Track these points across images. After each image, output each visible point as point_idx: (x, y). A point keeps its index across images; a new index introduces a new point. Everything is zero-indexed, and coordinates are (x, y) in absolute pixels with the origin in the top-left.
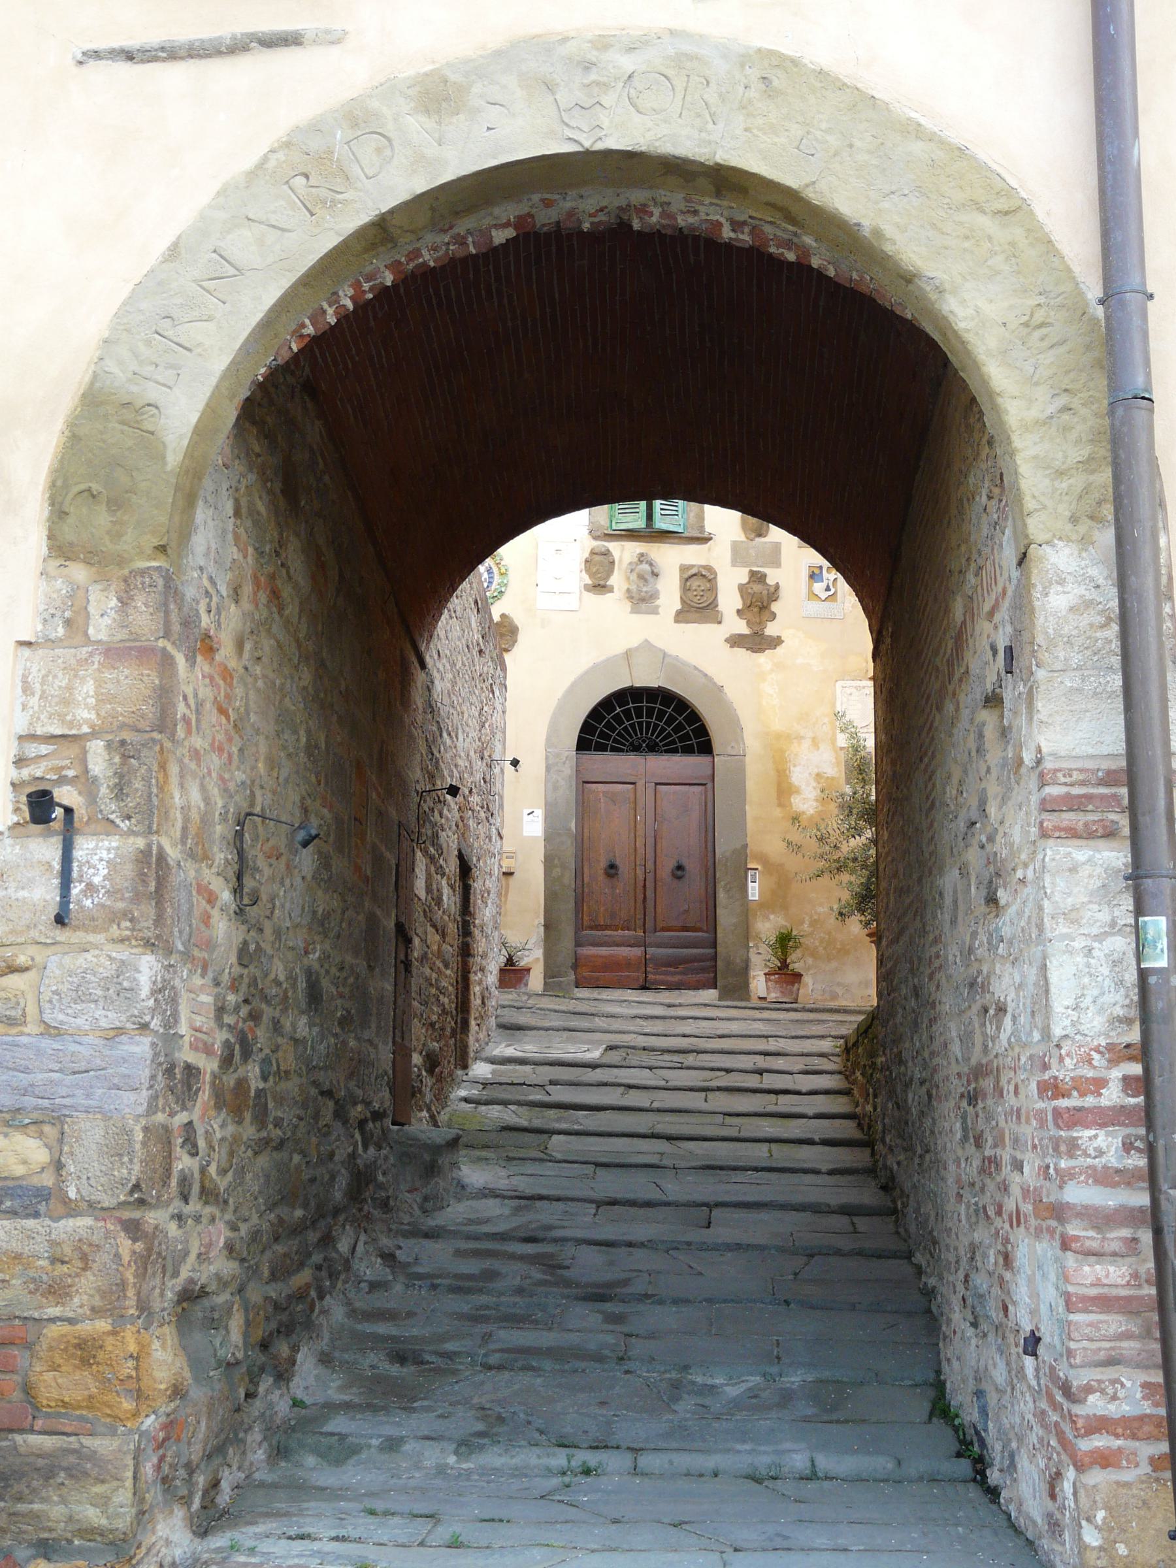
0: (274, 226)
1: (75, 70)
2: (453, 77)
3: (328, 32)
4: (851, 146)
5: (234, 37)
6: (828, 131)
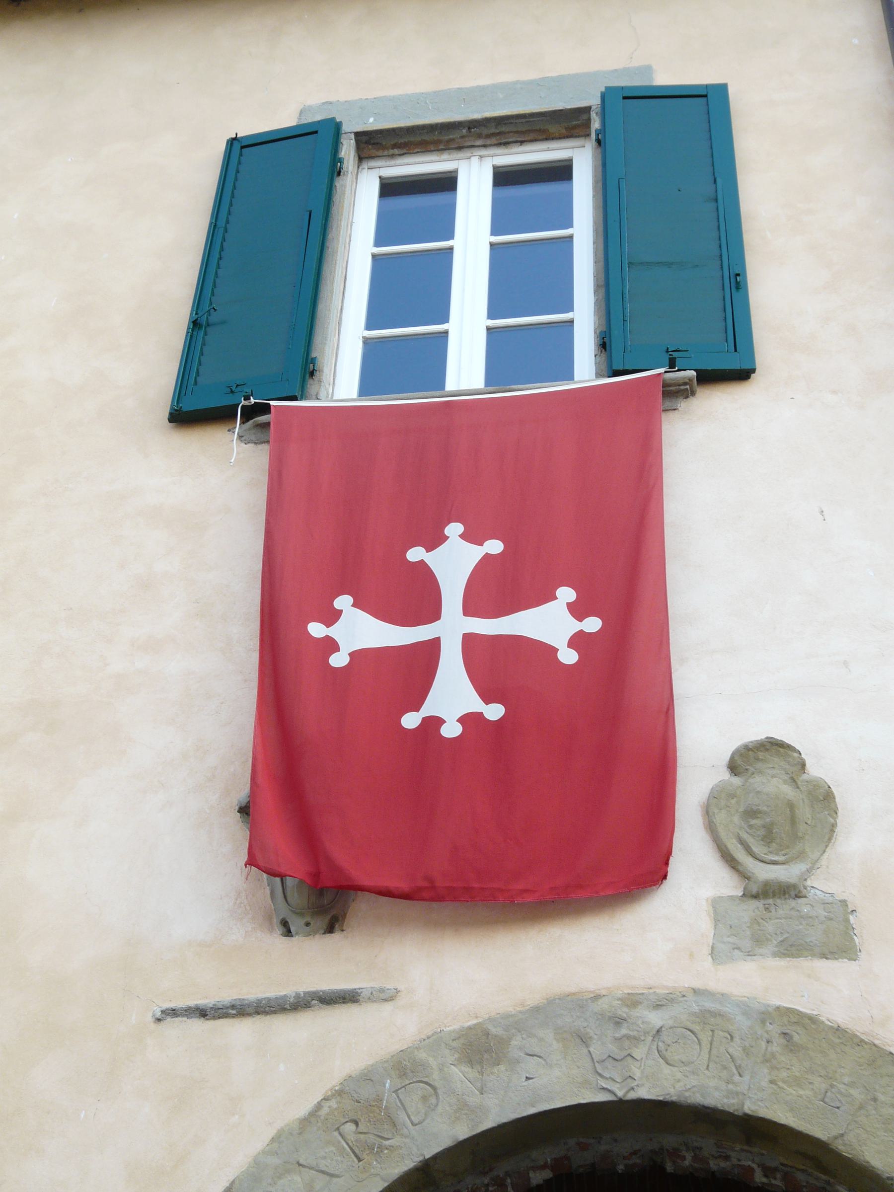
0: (323, 1172)
1: (153, 1026)
2: (493, 1030)
3: (382, 990)
4: (875, 1100)
5: (297, 996)
6: (852, 1085)
